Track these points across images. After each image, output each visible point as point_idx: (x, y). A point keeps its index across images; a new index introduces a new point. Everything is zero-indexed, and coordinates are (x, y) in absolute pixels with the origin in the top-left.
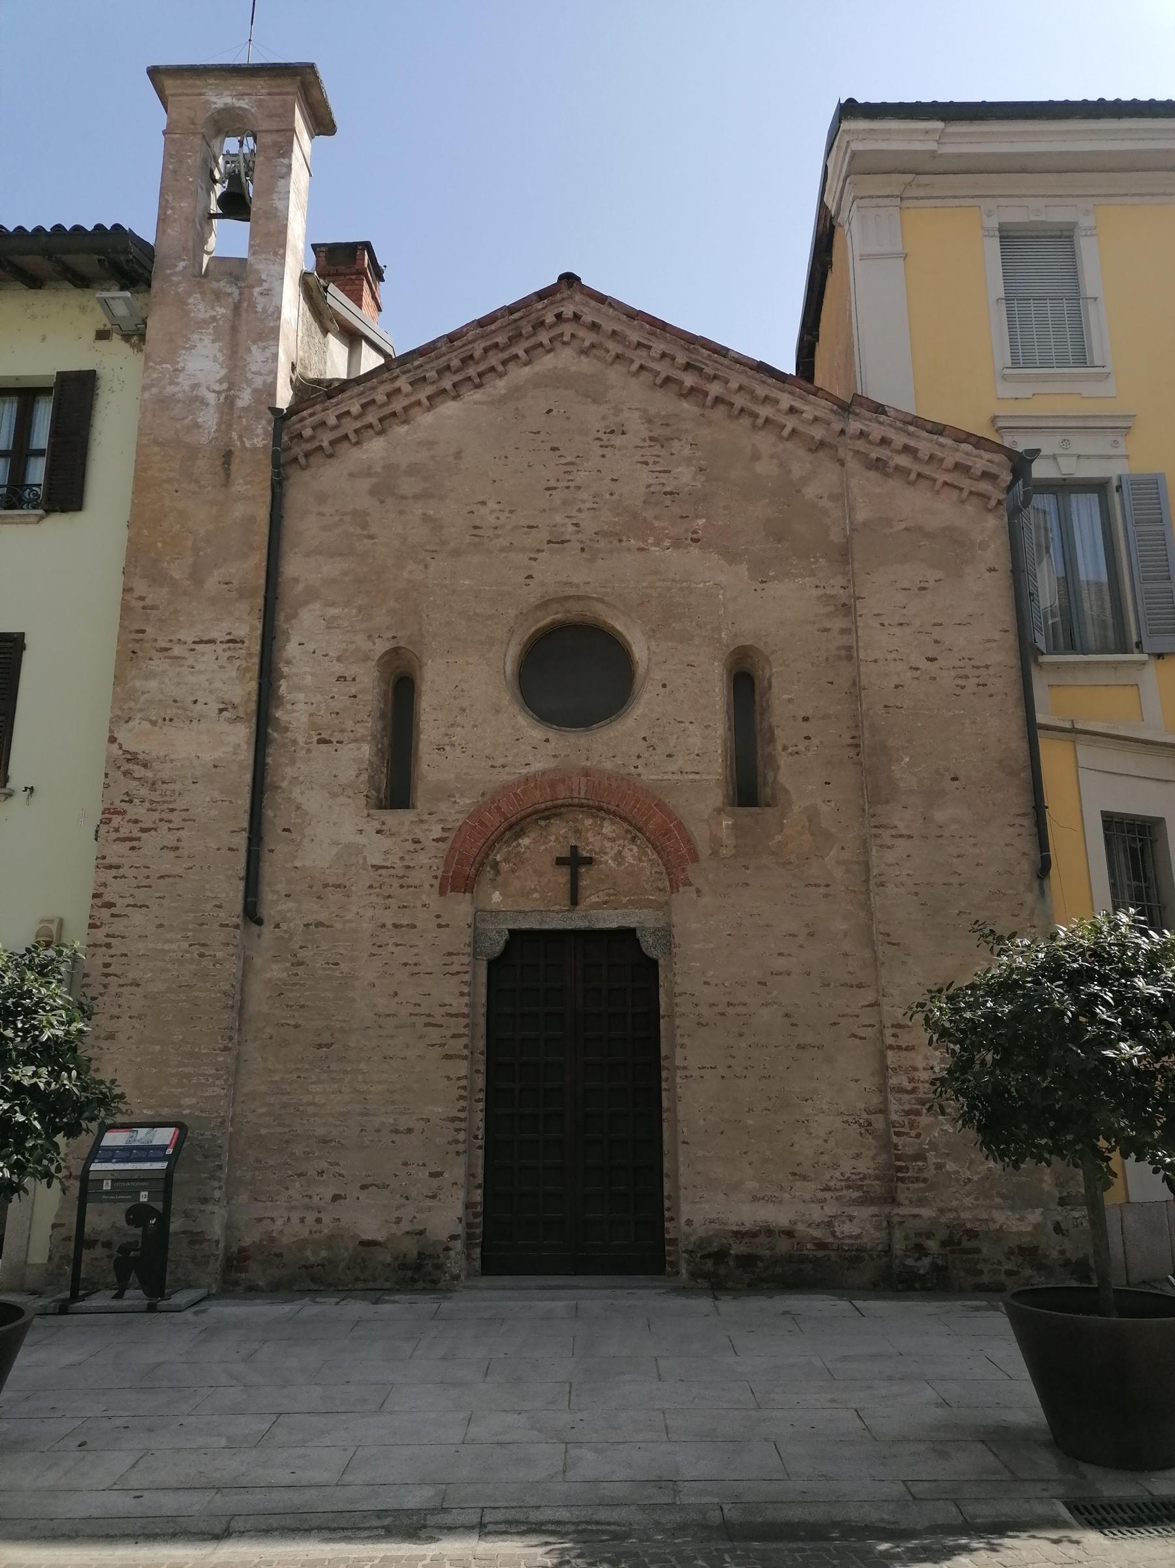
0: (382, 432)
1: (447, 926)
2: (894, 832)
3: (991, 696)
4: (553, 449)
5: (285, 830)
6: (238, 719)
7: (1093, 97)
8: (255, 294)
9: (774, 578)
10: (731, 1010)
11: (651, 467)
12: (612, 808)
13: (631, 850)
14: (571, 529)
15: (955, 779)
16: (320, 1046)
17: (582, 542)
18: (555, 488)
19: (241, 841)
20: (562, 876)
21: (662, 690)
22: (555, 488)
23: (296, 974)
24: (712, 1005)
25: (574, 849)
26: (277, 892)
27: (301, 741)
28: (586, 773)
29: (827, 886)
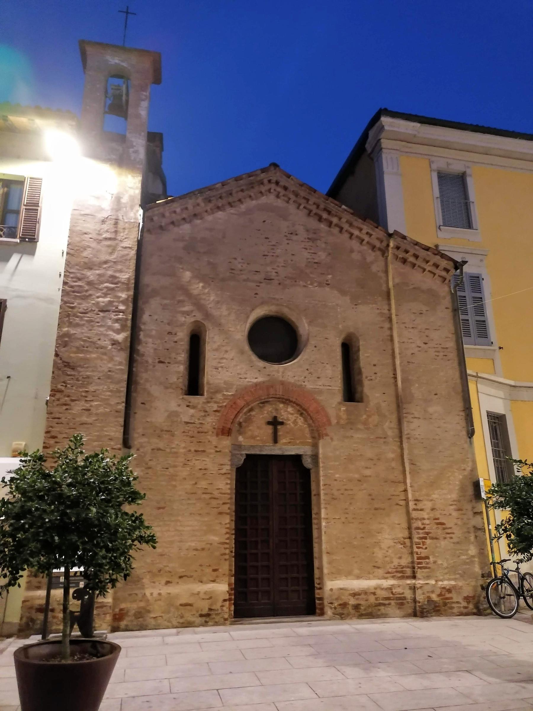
0: (190, 222)
1: (220, 451)
2: (412, 416)
3: (449, 360)
4: (267, 238)
5: (143, 403)
6: (122, 349)
7: (475, 124)
8: (130, 152)
9: (360, 304)
10: (346, 493)
11: (308, 251)
12: (294, 400)
13: (300, 419)
14: (274, 274)
15: (436, 394)
16: (159, 508)
17: (279, 280)
18: (267, 256)
19: (122, 407)
20: (269, 429)
21: (315, 349)
22: (267, 256)
23: (147, 473)
24: (338, 490)
25: (275, 418)
26: (138, 433)
27: (150, 361)
28: (282, 383)
29: (385, 438)
